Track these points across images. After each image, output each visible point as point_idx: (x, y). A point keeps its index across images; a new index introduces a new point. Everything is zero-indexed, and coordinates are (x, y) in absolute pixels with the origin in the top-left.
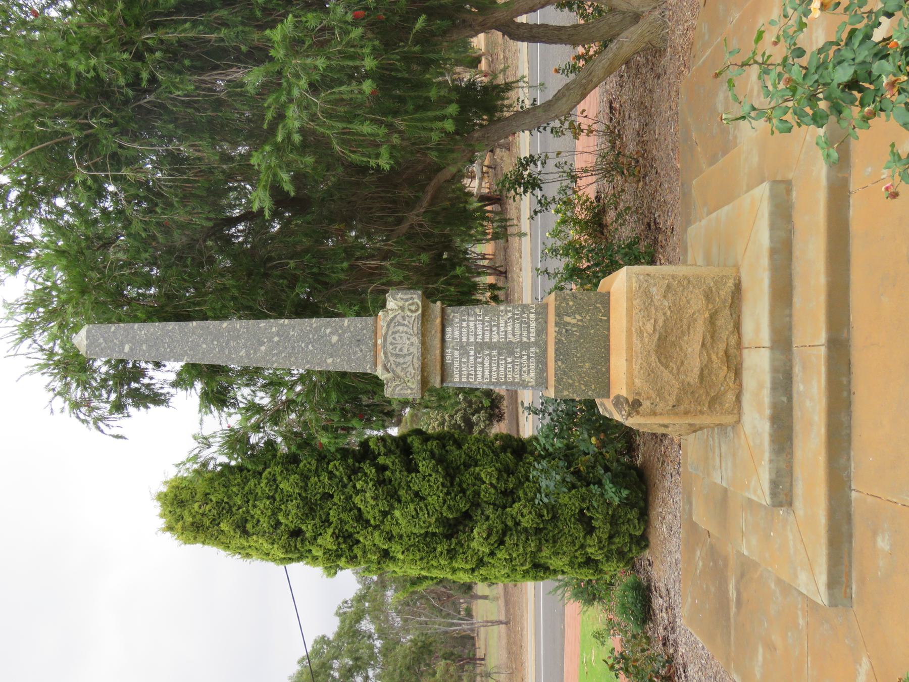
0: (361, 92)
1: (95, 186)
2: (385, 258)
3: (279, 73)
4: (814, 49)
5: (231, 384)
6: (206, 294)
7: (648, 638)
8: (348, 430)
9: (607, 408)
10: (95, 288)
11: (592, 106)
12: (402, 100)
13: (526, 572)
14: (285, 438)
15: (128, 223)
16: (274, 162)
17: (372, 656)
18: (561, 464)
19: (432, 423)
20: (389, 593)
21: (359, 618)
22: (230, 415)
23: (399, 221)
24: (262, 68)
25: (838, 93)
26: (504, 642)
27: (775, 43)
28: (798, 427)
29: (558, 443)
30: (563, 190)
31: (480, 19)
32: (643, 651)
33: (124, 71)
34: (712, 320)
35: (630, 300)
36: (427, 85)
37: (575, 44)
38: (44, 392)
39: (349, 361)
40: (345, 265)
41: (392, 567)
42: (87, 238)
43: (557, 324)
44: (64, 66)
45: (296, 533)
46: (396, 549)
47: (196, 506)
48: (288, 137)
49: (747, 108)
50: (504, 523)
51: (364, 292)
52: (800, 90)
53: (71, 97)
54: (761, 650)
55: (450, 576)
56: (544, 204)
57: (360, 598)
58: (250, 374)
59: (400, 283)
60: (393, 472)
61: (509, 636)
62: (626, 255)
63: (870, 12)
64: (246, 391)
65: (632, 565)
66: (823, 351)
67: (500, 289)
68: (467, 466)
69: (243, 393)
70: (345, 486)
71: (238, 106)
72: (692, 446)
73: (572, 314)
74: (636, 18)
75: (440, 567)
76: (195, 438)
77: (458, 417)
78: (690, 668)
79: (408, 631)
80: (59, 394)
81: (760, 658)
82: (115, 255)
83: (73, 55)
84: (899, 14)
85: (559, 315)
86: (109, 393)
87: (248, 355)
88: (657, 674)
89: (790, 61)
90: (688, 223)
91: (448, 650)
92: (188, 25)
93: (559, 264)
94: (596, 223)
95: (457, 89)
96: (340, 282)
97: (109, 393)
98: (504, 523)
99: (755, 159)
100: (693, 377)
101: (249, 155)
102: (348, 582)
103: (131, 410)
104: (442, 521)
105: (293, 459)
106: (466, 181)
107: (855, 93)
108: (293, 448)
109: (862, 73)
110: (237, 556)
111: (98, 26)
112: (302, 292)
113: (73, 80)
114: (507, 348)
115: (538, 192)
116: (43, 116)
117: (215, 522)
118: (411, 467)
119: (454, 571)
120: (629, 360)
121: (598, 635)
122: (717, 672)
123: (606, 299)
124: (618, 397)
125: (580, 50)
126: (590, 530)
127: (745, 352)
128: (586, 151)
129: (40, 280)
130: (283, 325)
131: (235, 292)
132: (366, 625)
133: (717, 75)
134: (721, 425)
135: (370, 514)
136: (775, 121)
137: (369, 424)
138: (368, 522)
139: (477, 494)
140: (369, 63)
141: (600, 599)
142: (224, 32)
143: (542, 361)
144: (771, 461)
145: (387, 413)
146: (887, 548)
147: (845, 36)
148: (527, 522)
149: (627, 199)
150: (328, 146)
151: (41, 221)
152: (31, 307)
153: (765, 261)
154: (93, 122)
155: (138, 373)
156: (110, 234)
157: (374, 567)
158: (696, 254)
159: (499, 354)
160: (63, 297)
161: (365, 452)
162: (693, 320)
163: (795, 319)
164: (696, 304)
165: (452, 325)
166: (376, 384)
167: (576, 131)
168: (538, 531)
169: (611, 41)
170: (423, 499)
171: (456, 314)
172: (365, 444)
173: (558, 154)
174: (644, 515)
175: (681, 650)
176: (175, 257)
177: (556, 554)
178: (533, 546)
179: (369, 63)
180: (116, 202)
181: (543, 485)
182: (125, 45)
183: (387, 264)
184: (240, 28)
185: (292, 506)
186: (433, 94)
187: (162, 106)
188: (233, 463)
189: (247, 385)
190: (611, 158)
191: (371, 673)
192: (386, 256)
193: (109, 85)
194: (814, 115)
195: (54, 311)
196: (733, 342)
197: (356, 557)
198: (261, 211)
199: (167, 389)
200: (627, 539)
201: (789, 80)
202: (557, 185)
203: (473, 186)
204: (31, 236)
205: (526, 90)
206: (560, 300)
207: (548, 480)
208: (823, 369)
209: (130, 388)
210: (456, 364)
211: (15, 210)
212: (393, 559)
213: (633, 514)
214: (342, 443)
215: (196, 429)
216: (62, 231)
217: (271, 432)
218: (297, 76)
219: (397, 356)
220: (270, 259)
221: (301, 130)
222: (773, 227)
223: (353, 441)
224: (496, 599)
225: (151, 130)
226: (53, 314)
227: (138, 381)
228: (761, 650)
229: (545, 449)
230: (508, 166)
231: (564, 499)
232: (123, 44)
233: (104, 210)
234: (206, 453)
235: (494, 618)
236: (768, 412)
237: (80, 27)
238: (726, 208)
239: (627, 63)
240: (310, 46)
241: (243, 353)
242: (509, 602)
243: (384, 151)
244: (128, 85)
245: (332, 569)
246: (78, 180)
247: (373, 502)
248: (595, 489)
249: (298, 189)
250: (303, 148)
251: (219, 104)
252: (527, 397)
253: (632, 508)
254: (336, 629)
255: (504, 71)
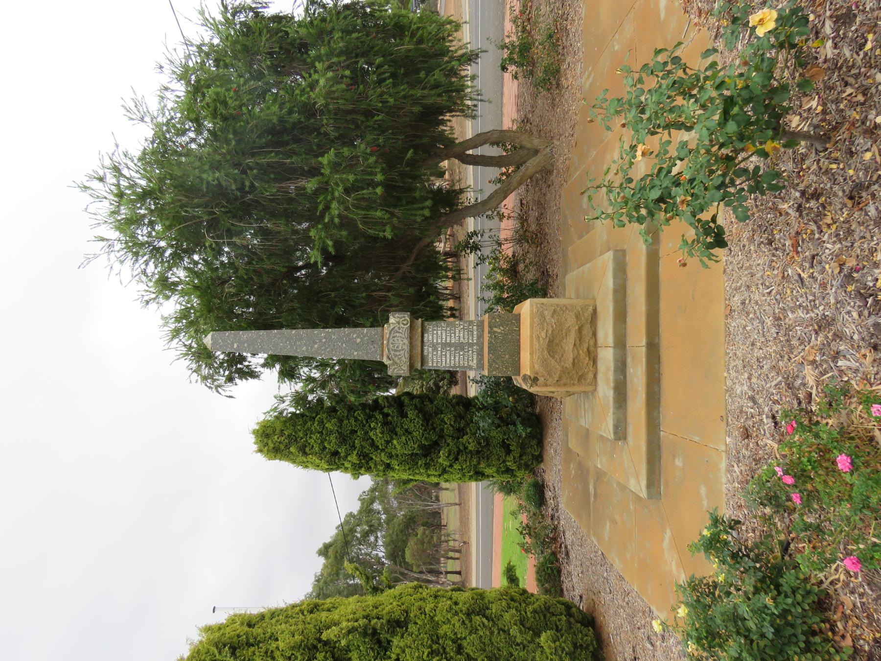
0: (376, 193)
1: (217, 249)
2: (388, 291)
3: (327, 182)
4: (639, 178)
5: (297, 366)
6: (282, 312)
7: (542, 515)
8: (366, 393)
9: (518, 381)
10: (217, 308)
11: (510, 203)
12: (399, 199)
13: (471, 477)
14: (329, 397)
15: (236, 270)
16: (323, 234)
17: (380, 524)
18: (492, 413)
19: (415, 388)
20: (390, 487)
21: (372, 502)
22: (296, 383)
23: (397, 269)
24: (316, 178)
25: (652, 205)
26: (458, 515)
27: (616, 174)
28: (630, 394)
29: (490, 401)
30: (493, 252)
31: (445, 152)
32: (540, 523)
33: (235, 180)
34: (580, 330)
35: (532, 318)
36: (414, 189)
37: (500, 167)
38: (186, 370)
39: (367, 354)
40: (364, 294)
41: (392, 474)
42: (212, 279)
43: (489, 333)
44: (200, 178)
45: (335, 454)
46: (394, 463)
47: (276, 437)
48: (332, 220)
49: (599, 213)
50: (458, 447)
51: (377, 310)
52: (630, 203)
53: (203, 196)
54: (608, 524)
55: (426, 479)
56: (482, 259)
57: (373, 490)
58: (308, 360)
59: (397, 306)
60: (393, 417)
61: (461, 512)
62: (530, 290)
63: (671, 158)
64: (306, 369)
65: (533, 472)
66: (644, 349)
67: (456, 310)
68: (436, 414)
69: (304, 371)
70: (364, 426)
71: (302, 201)
72: (568, 402)
73: (498, 326)
74: (536, 152)
75: (421, 474)
76: (275, 397)
77: (431, 383)
78: (567, 533)
79: (401, 510)
80: (195, 371)
81: (608, 528)
82: (229, 289)
83: (205, 171)
84: (686, 160)
85: (490, 327)
86: (224, 371)
87: (307, 349)
88: (548, 537)
89: (624, 185)
90: (566, 272)
91: (425, 520)
92: (273, 154)
93: (491, 294)
94: (513, 271)
95: (432, 191)
96: (361, 305)
97: (224, 371)
98: (458, 447)
99: (605, 237)
100: (569, 364)
101: (308, 230)
102: (366, 481)
103: (237, 381)
104: (422, 446)
105: (333, 410)
106: (437, 244)
107: (661, 204)
108: (334, 404)
109: (666, 194)
110: (300, 467)
111: (220, 154)
112: (340, 310)
113: (204, 186)
114: (460, 347)
115: (479, 253)
116: (187, 207)
117: (287, 447)
118: (404, 415)
119: (429, 476)
120: (531, 354)
121: (513, 514)
122: (583, 536)
123: (518, 318)
124: (525, 376)
125: (504, 170)
126: (508, 452)
127: (599, 350)
128: (507, 228)
129: (184, 303)
130: (328, 332)
131: (299, 311)
132: (377, 506)
133: (582, 193)
134: (584, 392)
135: (380, 442)
136: (616, 221)
137: (378, 388)
138: (378, 447)
139: (442, 430)
140: (379, 177)
141: (515, 492)
142: (294, 159)
143: (480, 354)
144: (614, 413)
145: (391, 382)
146: (681, 465)
147: (656, 171)
148: (471, 447)
149: (531, 257)
150: (356, 226)
151: (185, 268)
152: (178, 320)
153: (610, 297)
154: (216, 210)
155: (242, 359)
156: (225, 276)
157: (381, 474)
158: (570, 291)
159: (456, 350)
160: (198, 314)
161: (376, 406)
162: (569, 330)
163: (629, 331)
164: (570, 321)
165: (428, 333)
166: (382, 367)
167: (501, 217)
168: (478, 452)
169: (521, 165)
170: (410, 433)
171: (430, 326)
172: (376, 401)
173: (491, 230)
174: (540, 443)
175: (562, 522)
176: (263, 290)
177: (489, 466)
178: (475, 461)
179: (379, 177)
180: (229, 258)
181: (481, 425)
182: (236, 165)
183: (389, 294)
184: (304, 156)
185: (332, 438)
186: (417, 194)
187: (257, 202)
188: (298, 412)
189: (306, 366)
190: (521, 232)
191: (379, 534)
192: (389, 289)
193: (226, 189)
194: (638, 217)
195: (192, 322)
196: (592, 343)
197: (370, 467)
198: (316, 263)
199: (259, 369)
200: (530, 457)
201: (624, 197)
202: (490, 248)
203: (441, 247)
204: (178, 277)
205: (472, 194)
206: (492, 318)
207: (484, 422)
208: (644, 360)
209: (237, 368)
210: (430, 356)
211: (169, 261)
212: (393, 469)
213: (534, 442)
214: (363, 400)
215: (276, 392)
216: (197, 274)
217: (320, 393)
218: (337, 185)
219: (395, 351)
220: (320, 292)
221: (339, 216)
222: (615, 277)
223: (370, 399)
224: (453, 490)
225: (250, 215)
226: (191, 324)
227: (241, 364)
228: (608, 524)
229: (482, 404)
230: (462, 237)
231: (494, 433)
232: (236, 165)
233: (222, 263)
234: (282, 406)
235: (452, 501)
236: (612, 385)
237: (209, 155)
238: (588, 265)
239: (531, 178)
240: (345, 167)
241: (304, 348)
242: (461, 492)
243: (388, 228)
244: (237, 189)
245: (356, 475)
246: (207, 244)
247: (380, 435)
248: (511, 427)
249: (336, 251)
250: (341, 226)
251: (291, 200)
252: (472, 374)
253: (533, 439)
254: (358, 508)
255: (460, 180)
